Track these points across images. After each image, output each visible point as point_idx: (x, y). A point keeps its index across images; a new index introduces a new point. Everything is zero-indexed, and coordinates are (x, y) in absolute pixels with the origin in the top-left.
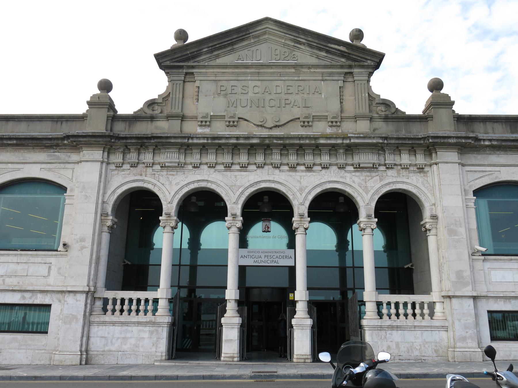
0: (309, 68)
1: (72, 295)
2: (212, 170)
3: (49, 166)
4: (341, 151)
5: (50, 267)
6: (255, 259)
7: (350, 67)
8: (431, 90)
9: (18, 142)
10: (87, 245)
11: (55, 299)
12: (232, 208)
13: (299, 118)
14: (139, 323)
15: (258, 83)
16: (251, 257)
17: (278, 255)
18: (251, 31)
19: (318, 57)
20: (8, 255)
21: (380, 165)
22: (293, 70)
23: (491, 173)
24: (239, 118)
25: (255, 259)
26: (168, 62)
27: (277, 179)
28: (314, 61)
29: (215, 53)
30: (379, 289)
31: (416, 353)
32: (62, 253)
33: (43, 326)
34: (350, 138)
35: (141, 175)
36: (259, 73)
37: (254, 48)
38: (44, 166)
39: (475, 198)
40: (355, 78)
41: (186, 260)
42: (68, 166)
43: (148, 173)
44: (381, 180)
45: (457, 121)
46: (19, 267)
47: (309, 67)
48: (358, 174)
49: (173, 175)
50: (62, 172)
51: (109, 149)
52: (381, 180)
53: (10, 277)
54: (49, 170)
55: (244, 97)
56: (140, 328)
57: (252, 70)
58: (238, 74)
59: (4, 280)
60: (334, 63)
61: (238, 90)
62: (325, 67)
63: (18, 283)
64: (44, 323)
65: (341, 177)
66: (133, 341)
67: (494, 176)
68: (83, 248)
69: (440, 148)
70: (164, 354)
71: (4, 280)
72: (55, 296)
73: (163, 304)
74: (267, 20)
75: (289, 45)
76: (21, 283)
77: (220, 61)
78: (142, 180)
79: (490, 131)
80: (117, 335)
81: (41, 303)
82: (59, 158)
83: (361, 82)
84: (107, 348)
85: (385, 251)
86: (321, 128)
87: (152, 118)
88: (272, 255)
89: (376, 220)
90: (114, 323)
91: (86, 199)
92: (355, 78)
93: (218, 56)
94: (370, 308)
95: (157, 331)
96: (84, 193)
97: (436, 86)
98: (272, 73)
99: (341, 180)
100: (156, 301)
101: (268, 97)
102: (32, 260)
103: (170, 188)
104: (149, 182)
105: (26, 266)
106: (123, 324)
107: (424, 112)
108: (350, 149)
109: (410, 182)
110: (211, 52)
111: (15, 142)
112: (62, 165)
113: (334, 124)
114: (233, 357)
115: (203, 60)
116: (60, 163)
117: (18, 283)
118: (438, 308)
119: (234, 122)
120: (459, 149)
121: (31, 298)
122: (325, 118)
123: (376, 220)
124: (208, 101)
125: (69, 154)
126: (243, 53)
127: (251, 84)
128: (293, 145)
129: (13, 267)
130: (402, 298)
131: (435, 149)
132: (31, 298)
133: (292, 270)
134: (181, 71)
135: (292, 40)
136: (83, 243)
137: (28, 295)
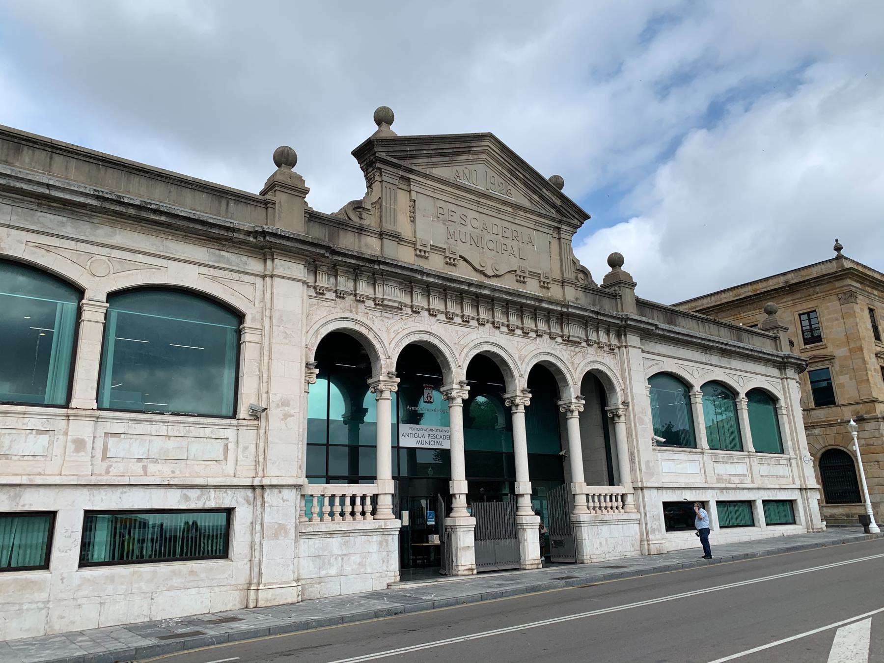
0: (526, 212)
1: (276, 491)
2: (434, 319)
3: (213, 272)
4: (325, 269)
5: (226, 446)
6: (418, 439)
7: (560, 222)
8: (278, 164)
9: (168, 220)
10: (292, 412)
11: (241, 500)
12: (458, 374)
13: (515, 271)
14: (365, 532)
15: (477, 215)
16: (414, 436)
17: (442, 434)
18: (473, 144)
19: (531, 200)
20: (151, 421)
21: (328, 290)
22: (510, 210)
23: (149, 267)
24: (460, 257)
25: (418, 439)
26: (384, 154)
27: (558, 353)
28: (526, 203)
29: (434, 160)
30: (589, 481)
31: (620, 549)
32: (244, 422)
33: (28, 552)
34: (568, 306)
35: (351, 312)
36: (478, 203)
37: (471, 167)
38: (204, 270)
39: (108, 305)
40: (384, 178)
41: (342, 437)
42: (244, 277)
43: (360, 310)
44: (584, 358)
45: (309, 220)
46: (171, 444)
47: (526, 210)
48: (565, 347)
49: (388, 318)
50: (237, 286)
51: (313, 267)
52: (584, 358)
53: (156, 461)
54: (214, 278)
55: (463, 229)
56: (364, 538)
57: (472, 197)
58: (458, 197)
59: (145, 468)
60: (543, 212)
61: (456, 218)
62: (540, 215)
63: (173, 472)
64: (31, 546)
65: (553, 349)
66: (356, 558)
67: (659, 366)
68: (286, 416)
69: (631, 332)
70: (398, 573)
71: (145, 468)
72: (241, 494)
73: (386, 503)
74: (490, 136)
75: (505, 176)
76: (177, 472)
77: (438, 172)
78: (355, 320)
79: (656, 318)
80: (336, 551)
81: (218, 506)
82: (228, 261)
83: (391, 186)
84: (323, 573)
85: (345, 422)
86: (532, 288)
87: (361, 230)
88: (436, 433)
89: (398, 380)
90: (331, 534)
91: (285, 338)
92: (384, 178)
93: (435, 165)
94: (581, 500)
95: (387, 541)
96: (281, 328)
97: (285, 159)
98: (490, 207)
99: (553, 352)
100: (375, 498)
101: (488, 237)
102: (194, 432)
103: (389, 338)
104: (363, 324)
105: (184, 443)
106: (345, 533)
107: (263, 193)
108: (563, 318)
109: (607, 364)
110: (430, 156)
111: (163, 218)
112: (235, 276)
113: (423, 253)
114: (472, 570)
115: (420, 164)
116: (232, 271)
117: (173, 472)
118: (630, 499)
119: (454, 260)
120: (306, 261)
121: (199, 498)
122: (538, 276)
123: (398, 380)
124: (427, 224)
125: (244, 258)
126: (460, 169)
127: (471, 214)
128: (421, 282)
129: (158, 443)
130: (358, 489)
131: (272, 255)
132: (199, 498)
133: (445, 455)
134: (395, 170)
135: (509, 170)
136: (286, 408)
137: (193, 493)
